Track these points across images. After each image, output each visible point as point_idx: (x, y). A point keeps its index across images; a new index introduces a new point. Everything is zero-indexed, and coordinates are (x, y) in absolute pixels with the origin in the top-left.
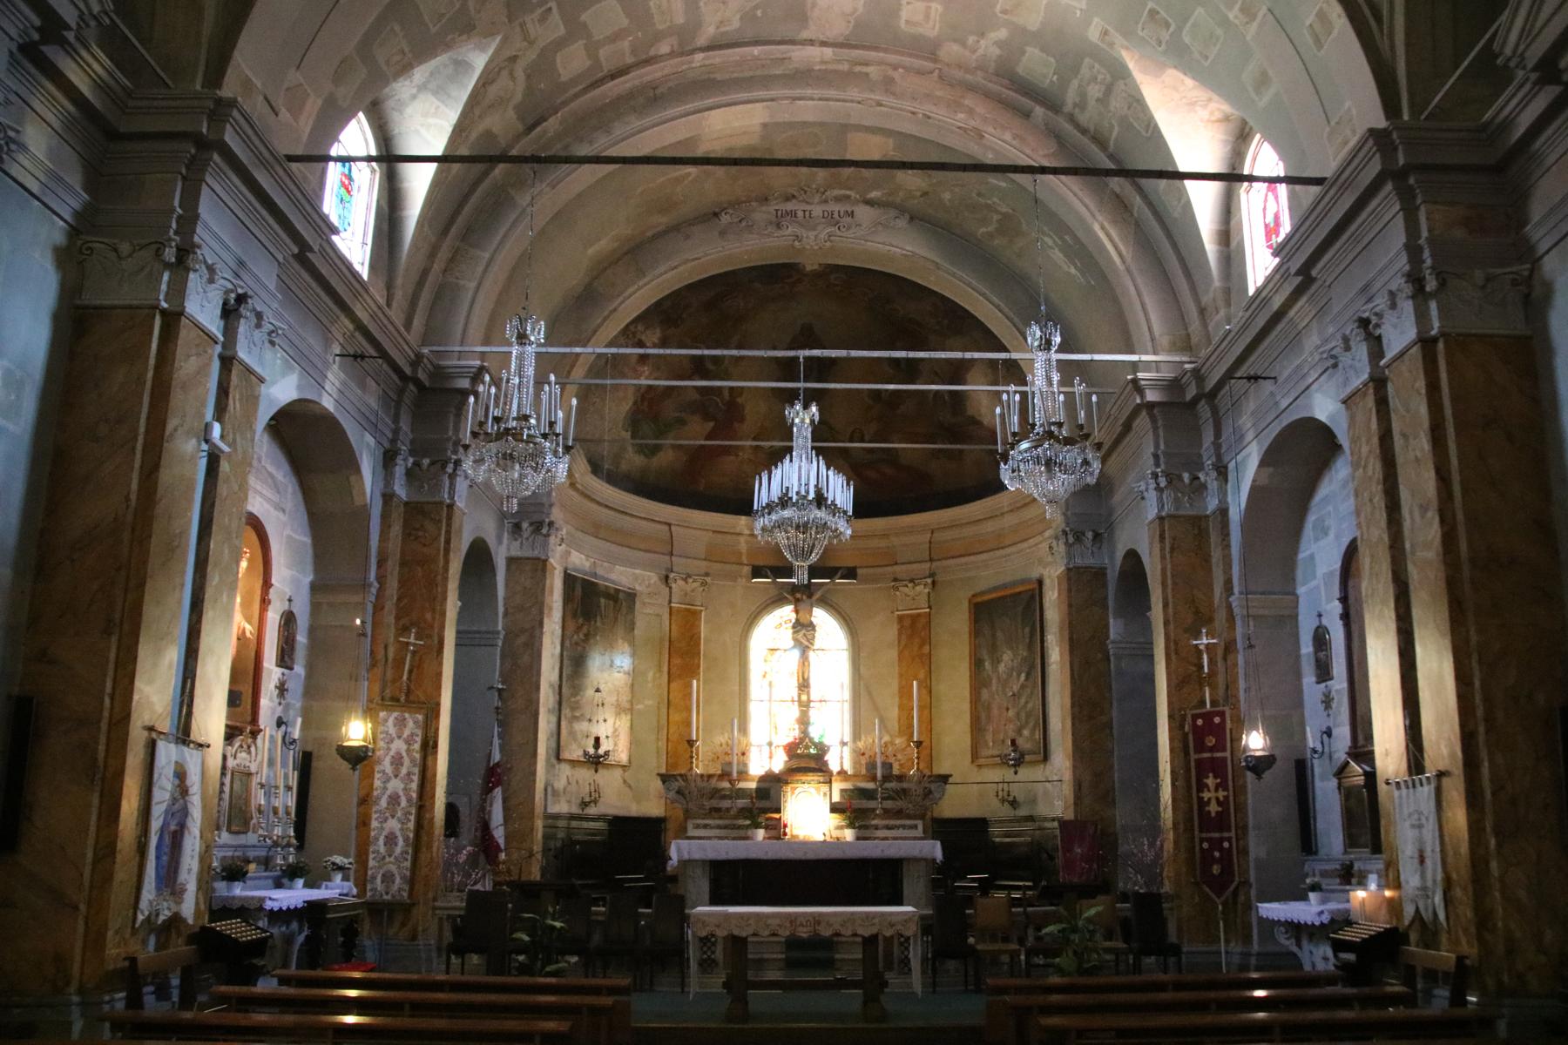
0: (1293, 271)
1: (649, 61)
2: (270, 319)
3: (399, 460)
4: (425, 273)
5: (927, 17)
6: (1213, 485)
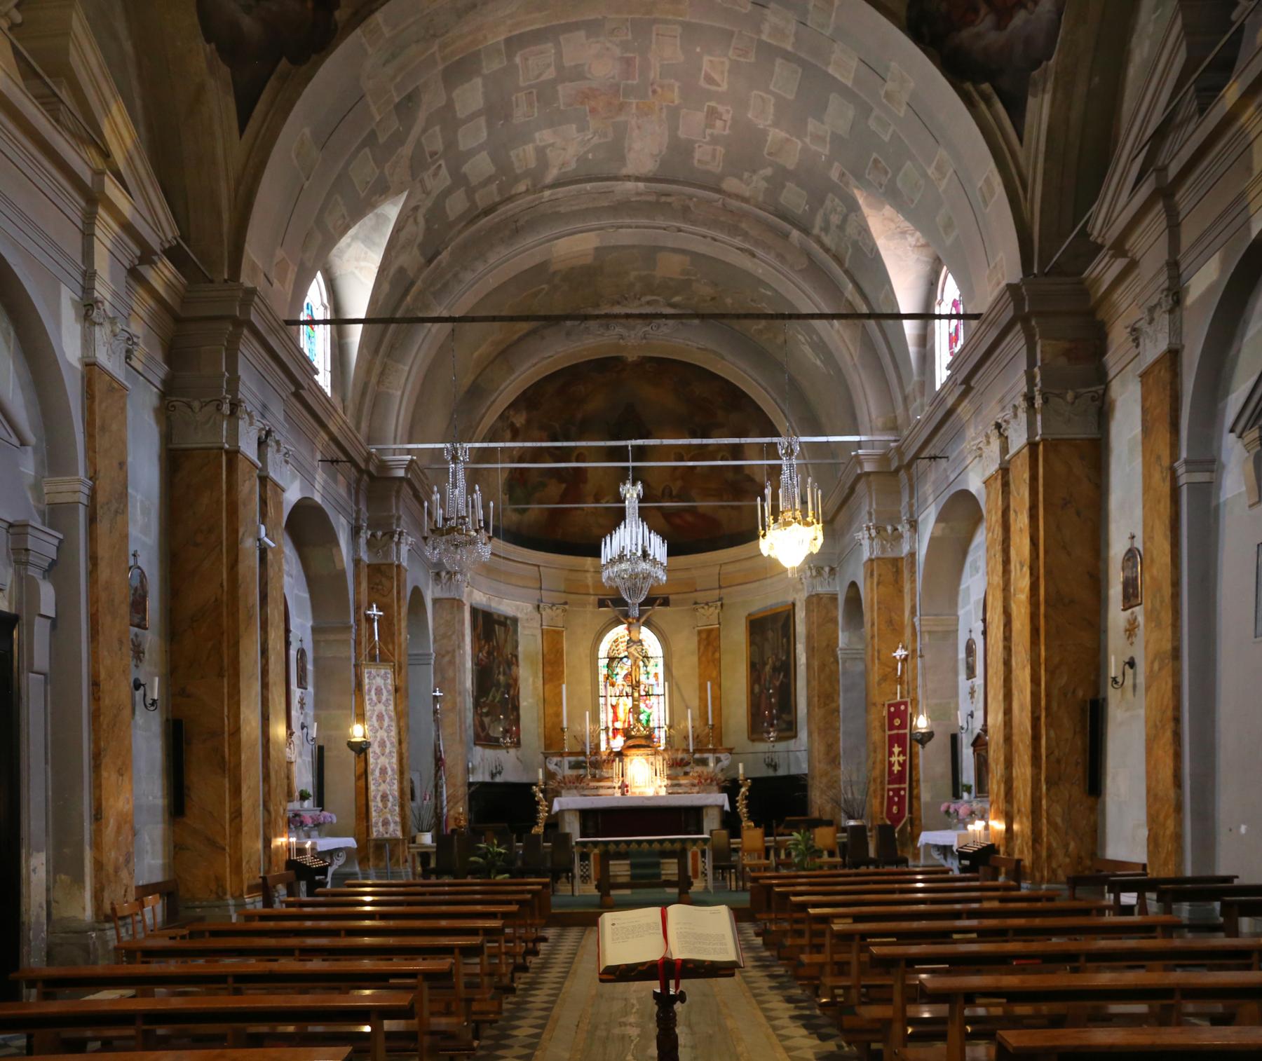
0: (959, 381)
1: (510, 199)
2: (285, 446)
3: (362, 534)
4: (366, 385)
5: (714, 156)
6: (907, 534)
